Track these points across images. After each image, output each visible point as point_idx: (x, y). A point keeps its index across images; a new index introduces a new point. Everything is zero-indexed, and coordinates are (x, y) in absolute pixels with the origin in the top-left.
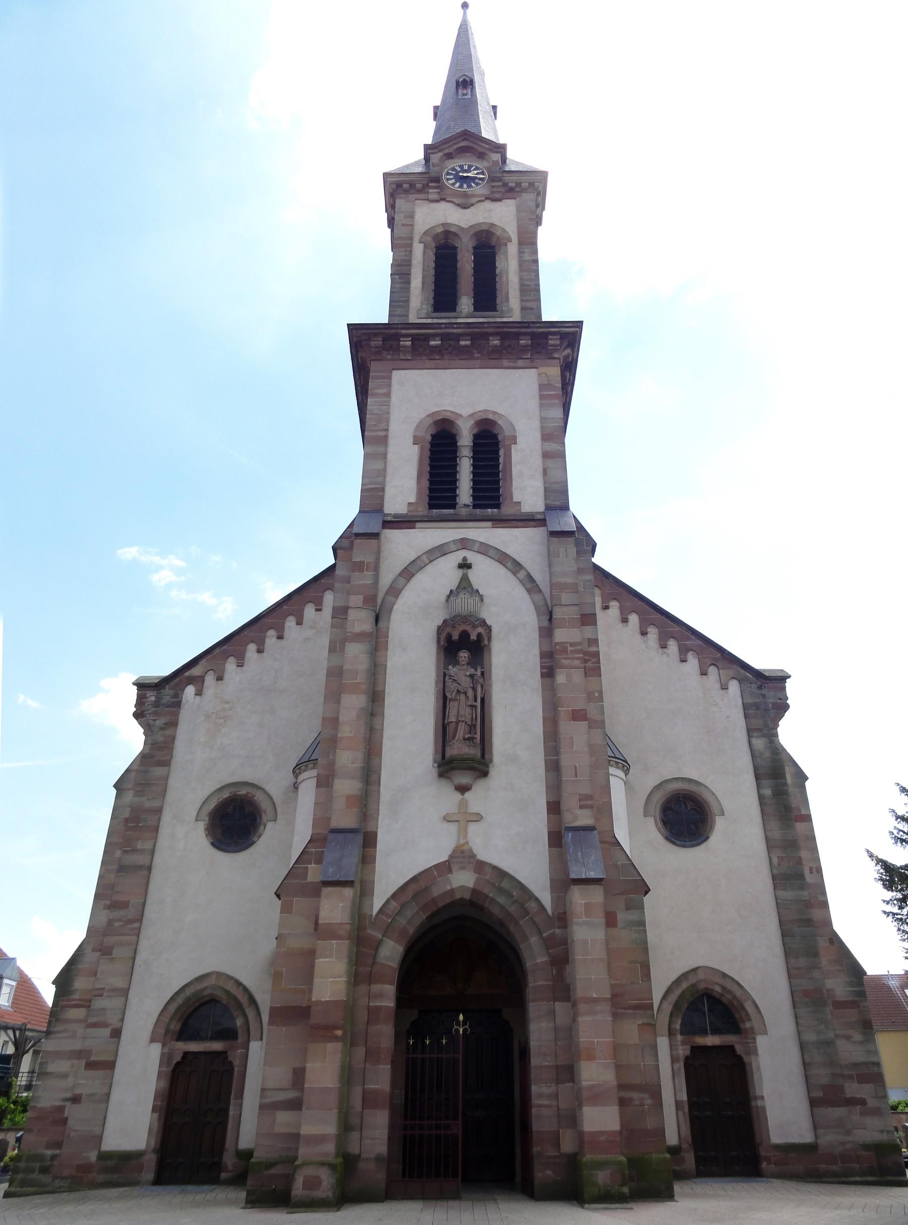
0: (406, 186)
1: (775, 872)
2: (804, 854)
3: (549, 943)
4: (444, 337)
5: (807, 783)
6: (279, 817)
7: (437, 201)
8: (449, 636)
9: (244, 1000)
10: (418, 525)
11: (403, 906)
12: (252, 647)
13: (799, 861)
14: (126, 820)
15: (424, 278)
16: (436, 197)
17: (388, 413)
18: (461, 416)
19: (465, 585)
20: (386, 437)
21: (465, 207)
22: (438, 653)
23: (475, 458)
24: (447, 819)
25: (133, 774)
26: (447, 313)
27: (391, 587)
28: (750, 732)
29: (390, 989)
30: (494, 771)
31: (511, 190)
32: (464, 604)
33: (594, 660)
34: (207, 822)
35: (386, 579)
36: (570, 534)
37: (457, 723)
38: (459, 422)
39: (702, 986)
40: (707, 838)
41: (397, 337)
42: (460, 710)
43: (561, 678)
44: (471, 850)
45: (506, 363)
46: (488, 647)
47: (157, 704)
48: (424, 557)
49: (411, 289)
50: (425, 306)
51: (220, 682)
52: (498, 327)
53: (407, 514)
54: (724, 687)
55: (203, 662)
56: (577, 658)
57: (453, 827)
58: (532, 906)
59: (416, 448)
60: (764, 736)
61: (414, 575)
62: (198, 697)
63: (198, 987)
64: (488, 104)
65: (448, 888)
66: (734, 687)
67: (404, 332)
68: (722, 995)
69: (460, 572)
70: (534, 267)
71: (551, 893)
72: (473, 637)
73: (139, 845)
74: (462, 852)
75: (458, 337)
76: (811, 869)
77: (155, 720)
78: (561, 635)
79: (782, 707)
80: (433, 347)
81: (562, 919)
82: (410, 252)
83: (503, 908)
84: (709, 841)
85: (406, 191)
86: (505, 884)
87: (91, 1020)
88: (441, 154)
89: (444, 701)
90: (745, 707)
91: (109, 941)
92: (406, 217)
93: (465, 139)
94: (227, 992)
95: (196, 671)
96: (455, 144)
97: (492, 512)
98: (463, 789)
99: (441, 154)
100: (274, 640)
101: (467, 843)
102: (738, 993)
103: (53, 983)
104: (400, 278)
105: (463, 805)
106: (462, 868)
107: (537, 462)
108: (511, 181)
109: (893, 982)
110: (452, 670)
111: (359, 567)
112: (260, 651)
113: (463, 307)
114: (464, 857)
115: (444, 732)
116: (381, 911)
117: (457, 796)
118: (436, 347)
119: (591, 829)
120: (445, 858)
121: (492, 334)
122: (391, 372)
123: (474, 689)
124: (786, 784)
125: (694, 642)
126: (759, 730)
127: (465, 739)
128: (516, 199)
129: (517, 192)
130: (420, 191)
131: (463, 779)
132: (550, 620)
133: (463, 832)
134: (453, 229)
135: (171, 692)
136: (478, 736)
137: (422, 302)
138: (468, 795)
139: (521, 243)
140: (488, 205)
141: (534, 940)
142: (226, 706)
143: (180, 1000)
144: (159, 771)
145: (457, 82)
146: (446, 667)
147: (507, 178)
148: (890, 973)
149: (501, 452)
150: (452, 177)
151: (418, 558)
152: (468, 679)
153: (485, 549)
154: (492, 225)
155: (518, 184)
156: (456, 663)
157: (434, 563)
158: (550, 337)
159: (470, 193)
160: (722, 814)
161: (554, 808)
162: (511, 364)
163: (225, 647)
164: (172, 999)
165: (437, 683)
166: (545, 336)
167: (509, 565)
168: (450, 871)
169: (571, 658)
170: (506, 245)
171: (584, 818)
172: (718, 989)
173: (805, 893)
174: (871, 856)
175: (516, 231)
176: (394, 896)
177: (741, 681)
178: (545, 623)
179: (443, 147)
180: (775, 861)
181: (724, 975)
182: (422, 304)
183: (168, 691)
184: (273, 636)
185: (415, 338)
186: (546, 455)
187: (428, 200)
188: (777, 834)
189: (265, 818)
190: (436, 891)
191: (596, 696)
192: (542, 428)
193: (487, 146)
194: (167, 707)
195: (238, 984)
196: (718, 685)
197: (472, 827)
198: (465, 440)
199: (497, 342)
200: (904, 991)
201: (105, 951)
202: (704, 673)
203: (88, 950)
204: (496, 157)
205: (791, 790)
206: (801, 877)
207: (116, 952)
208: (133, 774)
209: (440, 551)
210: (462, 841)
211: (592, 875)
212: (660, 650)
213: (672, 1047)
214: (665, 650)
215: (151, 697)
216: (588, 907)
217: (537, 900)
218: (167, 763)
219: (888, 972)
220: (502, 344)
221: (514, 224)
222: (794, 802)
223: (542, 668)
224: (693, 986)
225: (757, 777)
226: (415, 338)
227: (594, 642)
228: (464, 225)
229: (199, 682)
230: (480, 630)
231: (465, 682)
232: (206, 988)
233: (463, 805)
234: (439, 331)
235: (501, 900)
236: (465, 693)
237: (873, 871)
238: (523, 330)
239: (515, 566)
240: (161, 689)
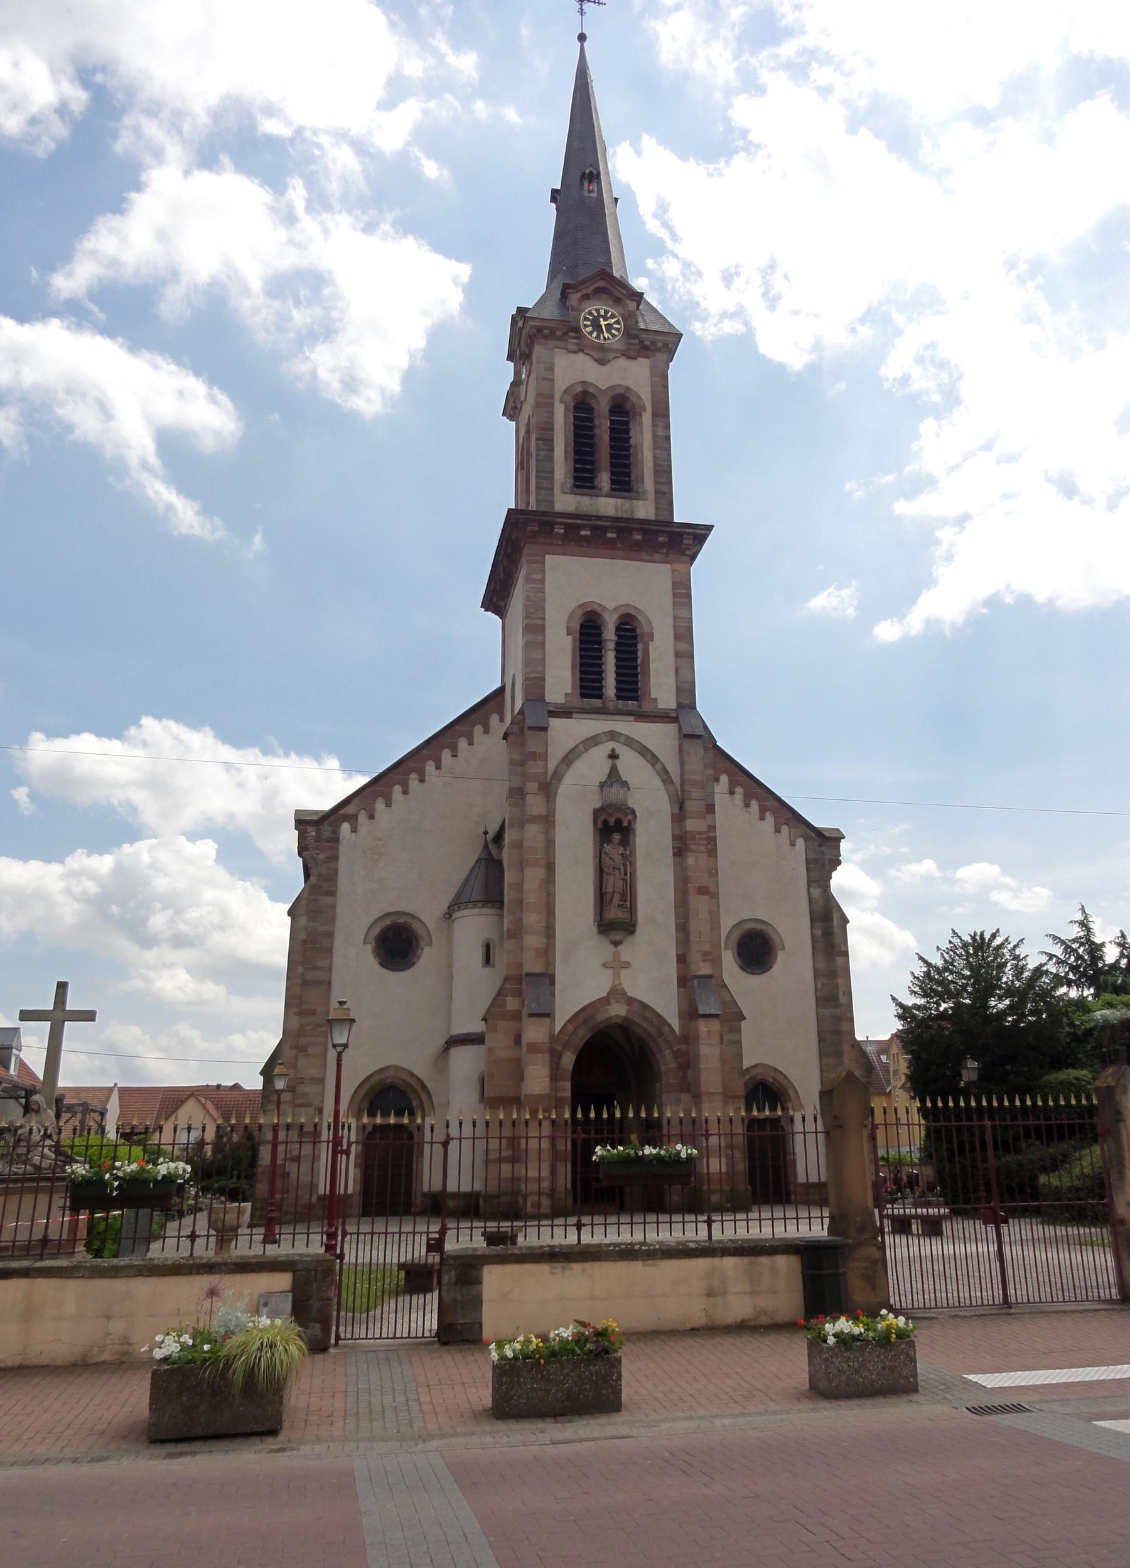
0: (546, 332)
1: (818, 994)
2: (841, 981)
3: (677, 1054)
4: (593, 528)
5: (848, 926)
6: (433, 942)
7: (575, 352)
8: (606, 822)
9: (418, 1087)
10: (574, 715)
11: (577, 1028)
12: (397, 789)
13: (836, 987)
14: (304, 942)
15: (566, 446)
16: (574, 347)
17: (544, 601)
18: (606, 609)
19: (613, 777)
20: (543, 626)
21: (602, 362)
22: (594, 832)
23: (617, 651)
24: (605, 965)
25: (304, 902)
26: (562, 447)
27: (555, 771)
28: (810, 883)
29: (568, 1085)
30: (639, 929)
31: (646, 348)
32: (615, 794)
33: (712, 843)
34: (374, 945)
35: (553, 763)
36: (699, 737)
37: (614, 892)
38: (606, 616)
39: (759, 1078)
40: (771, 967)
41: (552, 525)
42: (613, 883)
43: (690, 861)
44: (623, 989)
45: (644, 555)
46: (634, 831)
47: (318, 839)
48: (581, 747)
49: (555, 458)
50: (569, 480)
51: (372, 820)
52: (641, 524)
53: (564, 704)
55: (355, 801)
56: (703, 845)
57: (610, 972)
58: (666, 1028)
59: (569, 640)
60: (820, 887)
61: (573, 762)
62: (354, 834)
63: (383, 1076)
64: (612, 195)
65: (608, 1016)
66: (800, 843)
67: (559, 520)
68: (773, 1084)
69: (610, 761)
70: (666, 445)
71: (679, 1020)
72: (625, 824)
73: (319, 964)
74: (617, 990)
75: (605, 529)
76: (844, 993)
77: (318, 854)
78: (692, 825)
80: (582, 536)
81: (689, 1038)
82: (552, 414)
83: (646, 1030)
84: (772, 970)
85: (546, 337)
86: (647, 1014)
87: (298, 1102)
88: (578, 295)
89: (601, 872)
90: (808, 862)
91: (303, 1041)
92: (546, 369)
93: (602, 279)
94: (404, 1081)
95: (350, 809)
96: (593, 284)
97: (633, 705)
98: (616, 944)
99: (578, 295)
100: (416, 782)
101: (620, 984)
102: (784, 1083)
103: (261, 1073)
104: (544, 444)
105: (616, 955)
106: (618, 1002)
107: (671, 660)
108: (647, 339)
109: (870, 1048)
110: (608, 848)
111: (533, 756)
112: (405, 792)
113: (603, 484)
114: (618, 994)
115: (602, 899)
116: (561, 1031)
117: (612, 948)
118: (585, 537)
119: (710, 977)
120: (605, 994)
121: (635, 529)
122: (544, 556)
123: (625, 865)
124: (832, 927)
125: (771, 803)
126: (817, 881)
127: (619, 905)
128: (649, 358)
129: (651, 350)
130: (559, 339)
131: (617, 936)
132: (681, 808)
133: (617, 975)
134: (591, 390)
135: (329, 828)
136: (628, 903)
137: (566, 474)
138: (619, 948)
139: (655, 414)
140: (623, 362)
141: (667, 1052)
142: (379, 842)
143: (367, 1086)
144: (327, 900)
145: (583, 174)
146: (602, 845)
147: (643, 336)
148: (869, 1039)
149: (640, 646)
150: (589, 323)
151: (576, 747)
152: (620, 857)
153: (629, 742)
154: (628, 389)
155: (654, 343)
156: (609, 842)
157: (590, 751)
158: (685, 536)
159: (606, 346)
160: (783, 948)
161: (682, 959)
162: (649, 558)
163: (373, 788)
164: (360, 1086)
165: (595, 857)
166: (681, 535)
167: (649, 757)
168: (609, 1004)
169: (698, 844)
170: (641, 415)
171: (705, 969)
172: (771, 1080)
173: (838, 1011)
174: (894, 999)
175: (650, 398)
176: (570, 1021)
177: (806, 839)
178: (677, 811)
179: (581, 287)
180: (819, 986)
181: (776, 1070)
182: (566, 477)
183: (326, 828)
184: (415, 779)
185: (567, 527)
186: (677, 655)
187: (566, 349)
188: (821, 965)
189: (422, 943)
190: (600, 1018)
191: (713, 873)
192: (675, 627)
193: (624, 292)
194: (328, 842)
195: (412, 1074)
196: (788, 842)
197: (623, 972)
198: (610, 635)
199: (639, 537)
200: (879, 1056)
201: (301, 1049)
202: (778, 831)
203: (286, 1048)
204: (632, 305)
205: (837, 931)
206: (836, 998)
207: (310, 1050)
208: (304, 902)
209: (592, 741)
210: (618, 982)
211: (713, 1011)
212: (744, 809)
214: (748, 809)
215: (312, 832)
216: (709, 1032)
217: (669, 1025)
218: (333, 893)
219: (867, 1038)
220: (643, 537)
221: (649, 389)
222: (837, 940)
223: (673, 848)
224: (753, 1078)
225: (812, 920)
226: (567, 527)
227: (712, 828)
228: (603, 385)
229: (352, 819)
230: (630, 817)
231: (618, 859)
232: (387, 1078)
233: (616, 955)
234: (590, 522)
235: (645, 1025)
236: (619, 869)
237: (894, 1009)
238: (662, 529)
239: (653, 760)
240: (320, 825)
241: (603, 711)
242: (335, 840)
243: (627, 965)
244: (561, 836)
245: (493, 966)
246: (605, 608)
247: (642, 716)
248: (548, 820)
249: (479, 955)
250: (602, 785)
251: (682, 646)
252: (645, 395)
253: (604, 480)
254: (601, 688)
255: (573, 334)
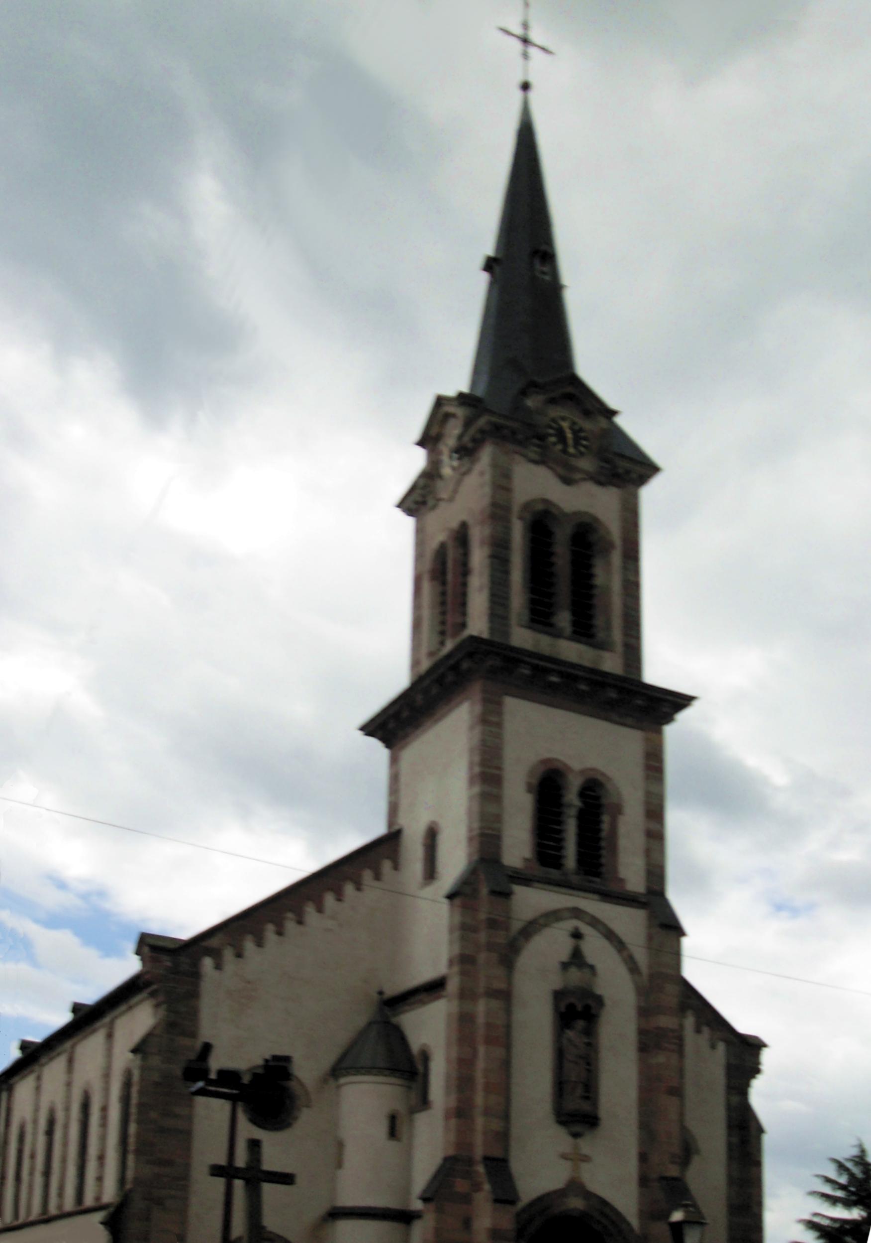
12: (270, 928)
16: (532, 456)
19: (577, 959)
21: (567, 481)
24: (564, 1157)
42: (574, 1073)
54: (713, 1047)
66: (721, 1047)
79: (754, 1070)
95: (214, 942)
98: (576, 1135)
110: (570, 1034)
115: (560, 1086)
117: (569, 1139)
130: (520, 443)
131: (577, 1128)
134: (554, 510)
140: (589, 487)
153: (595, 922)
198: (572, 797)
209: (553, 916)
213: (53, 1210)
229: (216, 955)
241: (564, 884)
242: (195, 975)
243: (586, 1159)
244: (519, 1015)
245: (399, 1140)
246: (569, 769)
247: (608, 896)
248: (505, 996)
249: (382, 1128)
250: (565, 966)
251: (653, 826)
252: (614, 529)
253: (564, 619)
254: (560, 857)
255: (536, 441)
